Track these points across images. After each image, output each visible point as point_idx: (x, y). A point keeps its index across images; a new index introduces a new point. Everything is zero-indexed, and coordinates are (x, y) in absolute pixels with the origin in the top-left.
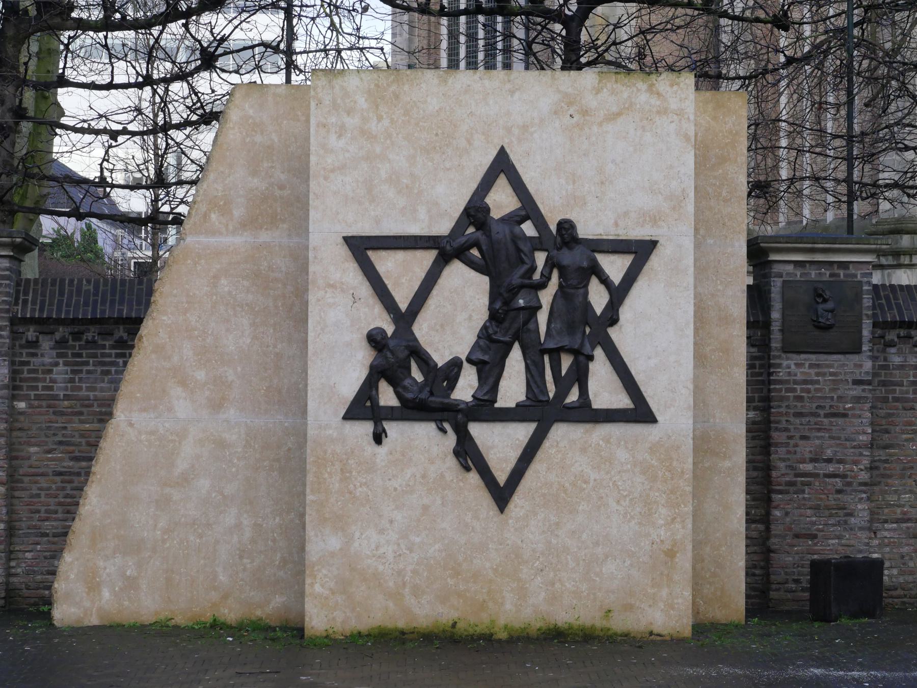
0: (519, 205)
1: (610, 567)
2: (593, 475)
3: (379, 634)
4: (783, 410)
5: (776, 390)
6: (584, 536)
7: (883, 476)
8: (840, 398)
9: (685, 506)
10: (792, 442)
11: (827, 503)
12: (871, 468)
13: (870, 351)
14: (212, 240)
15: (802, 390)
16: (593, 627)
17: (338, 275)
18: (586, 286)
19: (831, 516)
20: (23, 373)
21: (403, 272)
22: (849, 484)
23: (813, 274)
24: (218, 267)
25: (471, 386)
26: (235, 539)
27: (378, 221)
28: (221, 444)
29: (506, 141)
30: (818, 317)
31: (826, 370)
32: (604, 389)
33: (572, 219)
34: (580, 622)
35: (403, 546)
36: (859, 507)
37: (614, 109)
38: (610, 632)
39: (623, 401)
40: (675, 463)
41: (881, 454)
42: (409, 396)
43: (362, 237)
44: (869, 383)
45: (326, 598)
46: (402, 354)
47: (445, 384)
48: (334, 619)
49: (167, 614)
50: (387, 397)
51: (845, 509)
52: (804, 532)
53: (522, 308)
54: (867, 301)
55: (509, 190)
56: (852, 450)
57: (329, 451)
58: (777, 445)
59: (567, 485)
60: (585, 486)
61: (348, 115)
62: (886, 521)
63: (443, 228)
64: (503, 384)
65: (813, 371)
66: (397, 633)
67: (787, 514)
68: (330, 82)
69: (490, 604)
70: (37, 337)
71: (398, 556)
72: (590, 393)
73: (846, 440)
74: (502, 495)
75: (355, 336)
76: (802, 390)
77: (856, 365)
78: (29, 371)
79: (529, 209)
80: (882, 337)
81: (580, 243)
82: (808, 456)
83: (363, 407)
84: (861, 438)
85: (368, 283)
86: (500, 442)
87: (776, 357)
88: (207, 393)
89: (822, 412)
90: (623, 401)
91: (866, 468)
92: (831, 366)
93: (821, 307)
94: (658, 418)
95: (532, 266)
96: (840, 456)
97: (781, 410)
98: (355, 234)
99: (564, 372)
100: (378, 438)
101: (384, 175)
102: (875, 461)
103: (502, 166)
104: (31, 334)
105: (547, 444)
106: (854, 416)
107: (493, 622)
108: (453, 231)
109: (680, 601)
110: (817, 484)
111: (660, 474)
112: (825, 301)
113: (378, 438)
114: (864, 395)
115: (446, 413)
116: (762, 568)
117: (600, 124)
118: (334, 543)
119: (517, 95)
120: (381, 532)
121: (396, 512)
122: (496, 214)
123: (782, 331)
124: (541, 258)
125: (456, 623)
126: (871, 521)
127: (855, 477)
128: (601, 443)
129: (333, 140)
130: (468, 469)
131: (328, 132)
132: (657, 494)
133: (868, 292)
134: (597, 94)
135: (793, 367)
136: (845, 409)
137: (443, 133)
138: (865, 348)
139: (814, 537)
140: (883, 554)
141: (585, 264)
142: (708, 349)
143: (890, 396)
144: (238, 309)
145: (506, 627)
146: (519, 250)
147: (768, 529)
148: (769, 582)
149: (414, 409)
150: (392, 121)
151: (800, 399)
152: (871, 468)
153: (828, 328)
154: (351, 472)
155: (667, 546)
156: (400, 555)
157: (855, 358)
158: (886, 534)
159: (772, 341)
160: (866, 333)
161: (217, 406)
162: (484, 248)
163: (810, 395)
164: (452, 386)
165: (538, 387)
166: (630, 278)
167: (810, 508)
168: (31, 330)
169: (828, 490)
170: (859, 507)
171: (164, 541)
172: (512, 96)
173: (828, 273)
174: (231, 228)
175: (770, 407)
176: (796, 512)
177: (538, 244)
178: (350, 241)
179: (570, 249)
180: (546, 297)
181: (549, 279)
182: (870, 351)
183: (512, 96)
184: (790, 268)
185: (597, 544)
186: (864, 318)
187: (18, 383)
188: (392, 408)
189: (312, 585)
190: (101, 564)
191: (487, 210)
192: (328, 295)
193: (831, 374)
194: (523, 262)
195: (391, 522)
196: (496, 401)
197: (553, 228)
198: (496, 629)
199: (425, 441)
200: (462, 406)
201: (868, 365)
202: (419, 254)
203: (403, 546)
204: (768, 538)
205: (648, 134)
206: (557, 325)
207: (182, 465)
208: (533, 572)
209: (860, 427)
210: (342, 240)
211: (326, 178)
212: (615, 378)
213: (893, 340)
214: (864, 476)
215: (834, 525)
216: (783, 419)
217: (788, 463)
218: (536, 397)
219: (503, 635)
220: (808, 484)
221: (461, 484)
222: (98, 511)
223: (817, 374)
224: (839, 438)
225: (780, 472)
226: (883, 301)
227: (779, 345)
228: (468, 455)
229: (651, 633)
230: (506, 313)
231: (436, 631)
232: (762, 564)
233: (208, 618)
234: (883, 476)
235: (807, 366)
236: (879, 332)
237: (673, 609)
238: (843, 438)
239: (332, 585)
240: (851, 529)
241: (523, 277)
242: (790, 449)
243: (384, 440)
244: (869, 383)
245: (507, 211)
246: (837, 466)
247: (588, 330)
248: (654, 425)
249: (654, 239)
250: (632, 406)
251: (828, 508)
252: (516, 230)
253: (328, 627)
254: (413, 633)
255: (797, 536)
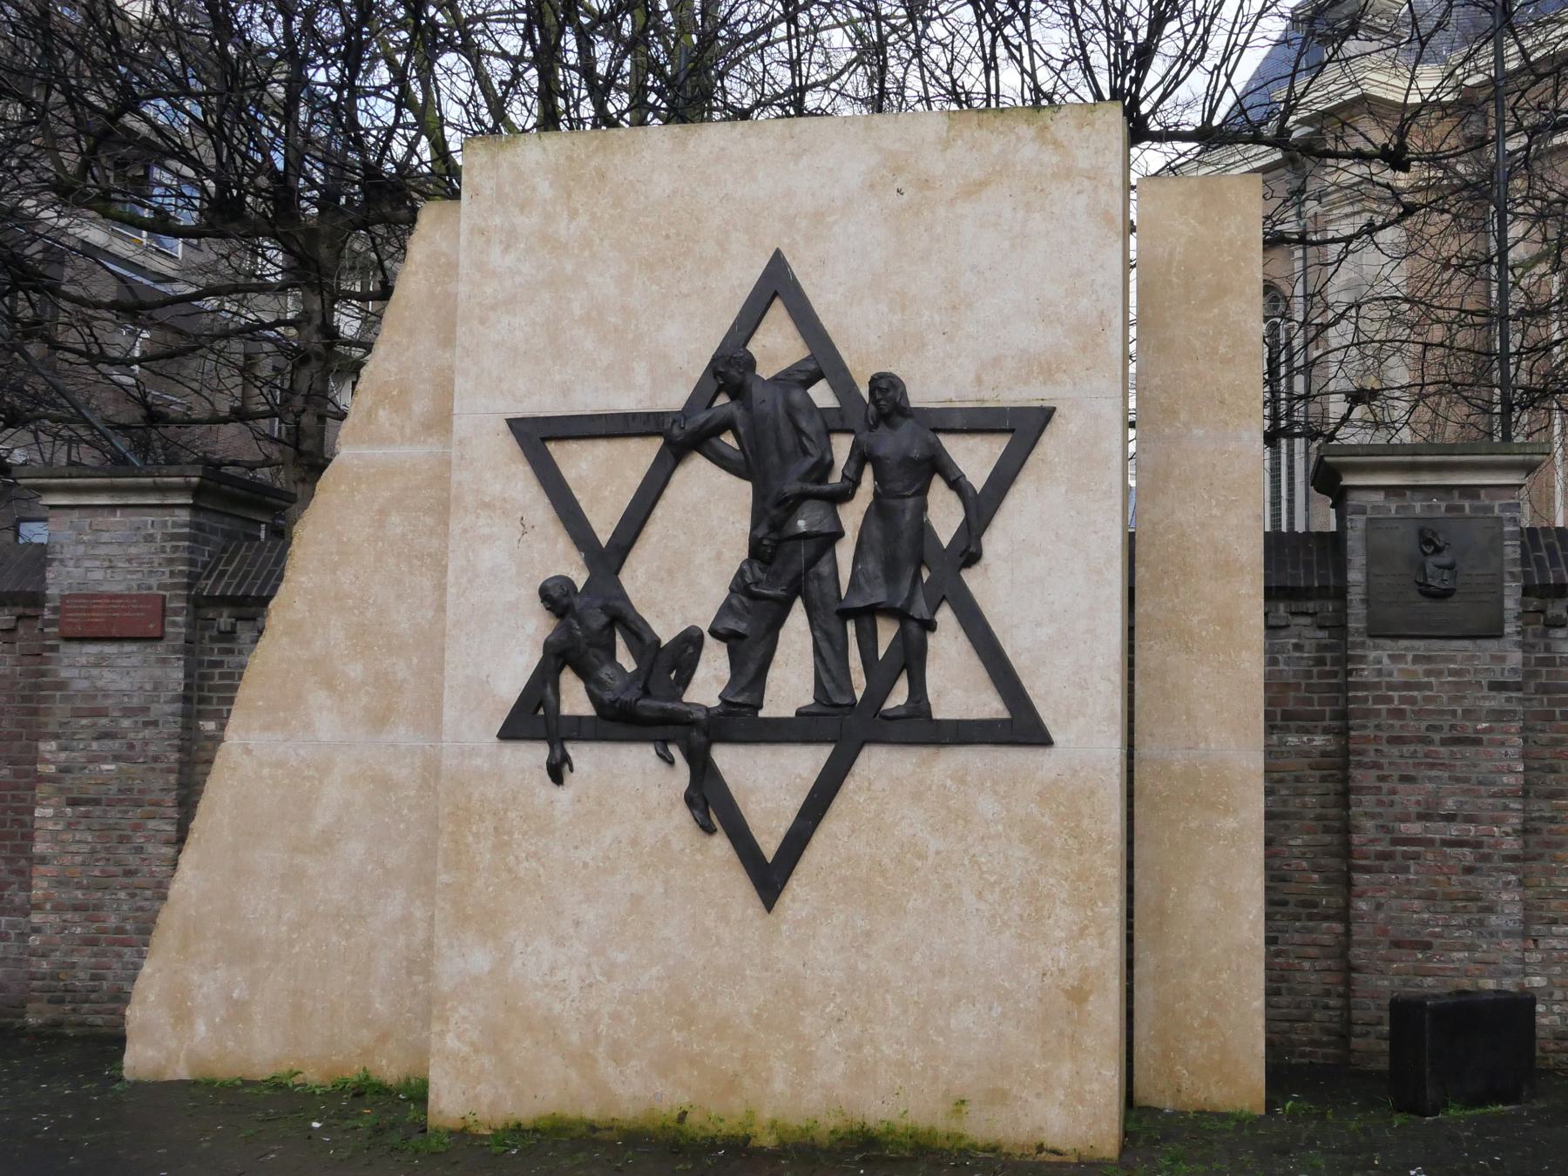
0: (807, 353)
1: (964, 1018)
2: (934, 844)
3: (553, 1128)
4: (1370, 732)
5: (1356, 699)
6: (917, 958)
7: (1548, 845)
8: (1467, 713)
9: (1105, 904)
10: (1385, 786)
11: (1449, 889)
12: (1525, 831)
13: (1518, 633)
14: (379, 452)
15: (1403, 700)
16: (931, 1130)
17: (498, 487)
18: (923, 491)
19: (1455, 911)
20: (212, 678)
21: (604, 476)
22: (1486, 858)
23: (1418, 508)
24: (387, 494)
25: (716, 678)
26: (401, 941)
27: (565, 389)
28: (385, 784)
29: (786, 241)
30: (1425, 578)
31: (1442, 666)
32: (954, 683)
33: (898, 373)
34: (907, 1122)
35: (595, 969)
36: (1505, 897)
37: (976, 175)
38: (963, 1144)
39: (991, 706)
40: (1086, 823)
41: (1542, 808)
42: (608, 696)
43: (536, 420)
44: (1518, 687)
45: (465, 1060)
46: (598, 620)
47: (673, 676)
48: (476, 1097)
49: (292, 1064)
50: (575, 699)
51: (1479, 899)
52: (1408, 937)
53: (804, 536)
54: (1512, 551)
55: (789, 327)
56: (1490, 801)
57: (476, 795)
58: (1360, 790)
59: (886, 861)
60: (919, 864)
61: (522, 209)
62: (1554, 922)
63: (674, 398)
64: (774, 674)
65: (1420, 668)
66: (584, 1129)
67: (1379, 907)
68: (493, 157)
69: (747, 1081)
70: (233, 626)
71: (587, 986)
72: (929, 691)
73: (1480, 783)
74: (769, 877)
75: (523, 592)
76: (1403, 700)
77: (1493, 657)
78: (222, 676)
79: (822, 360)
80: (1542, 611)
81: (911, 416)
82: (1413, 809)
83: (532, 718)
84: (1505, 780)
85: (547, 500)
86: (768, 781)
87: (1355, 645)
88: (365, 700)
89: (1437, 737)
90: (991, 706)
91: (1515, 831)
92: (1452, 660)
93: (1431, 562)
94: (1054, 737)
95: (822, 458)
96: (1468, 810)
97: (1367, 732)
98: (527, 415)
99: (881, 653)
100: (557, 771)
101: (577, 310)
102: (1532, 819)
103: (778, 285)
104: (224, 621)
105: (850, 784)
106: (1492, 742)
107: (750, 1114)
108: (690, 402)
109: (1096, 1087)
110: (1430, 856)
111: (1058, 843)
112: (1438, 550)
113: (557, 771)
114: (1508, 707)
115: (670, 728)
116: (1340, 996)
117: (952, 202)
118: (480, 960)
119: (805, 161)
120: (560, 942)
121: (584, 906)
122: (766, 370)
123: (1366, 602)
124: (842, 447)
125: (685, 1113)
126: (1526, 922)
127: (1497, 845)
128: (949, 782)
129: (496, 258)
130: (709, 830)
131: (488, 241)
132: (1052, 881)
133: (1512, 535)
134: (944, 150)
135: (1386, 660)
136: (1477, 731)
137: (678, 234)
138: (1509, 629)
139: (1427, 946)
140: (1549, 977)
141: (916, 453)
142: (1195, 620)
143: (1557, 710)
144: (415, 561)
145: (773, 1124)
146: (799, 431)
147: (1348, 933)
148: (1349, 1023)
149: (619, 721)
150: (593, 217)
151: (1399, 714)
152: (1525, 831)
153: (1444, 595)
154: (510, 833)
155: (1070, 981)
156: (590, 985)
157: (1491, 645)
158: (1555, 943)
159: (1351, 618)
160: (1511, 603)
161: (379, 720)
162: (741, 430)
163: (1416, 708)
164: (685, 680)
165: (833, 679)
166: (1004, 477)
167: (1418, 898)
168: (225, 614)
169: (1450, 867)
170: (1505, 897)
171: (291, 944)
172: (796, 163)
173: (1443, 505)
174: (408, 431)
175: (1349, 729)
176: (1395, 903)
177: (832, 423)
178: (518, 426)
179: (892, 426)
180: (852, 516)
181: (856, 483)
182: (1518, 633)
183: (796, 163)
184: (1378, 498)
185: (939, 973)
186: (1507, 577)
187: (206, 694)
188: (580, 718)
189: (442, 1034)
190: (195, 977)
191: (751, 363)
192: (482, 522)
193: (1452, 673)
194: (806, 452)
195: (577, 924)
196: (761, 707)
197: (864, 391)
198: (756, 1129)
199: (633, 780)
200: (701, 715)
201: (1515, 658)
202: (634, 445)
203: (595, 969)
204: (1348, 947)
205: (1037, 215)
206: (872, 565)
207: (322, 818)
208: (823, 1022)
209: (1505, 762)
210: (505, 426)
211: (482, 322)
212: (974, 661)
213: (1559, 616)
214: (1512, 845)
215: (1460, 927)
216: (1371, 748)
217: (1380, 822)
218: (828, 698)
219: (768, 1141)
220: (1415, 857)
221: (699, 857)
222: (193, 892)
223: (1428, 673)
224: (1466, 780)
225: (1367, 834)
226: (1544, 553)
227: (1361, 625)
228: (710, 802)
229: (1040, 1148)
230: (778, 544)
231: (651, 1127)
232: (1341, 989)
233: (353, 1073)
234: (1548, 845)
235: (1410, 658)
236: (1535, 603)
237: (1082, 1101)
238: (1474, 780)
239: (475, 1035)
240: (1491, 935)
241: (805, 478)
242: (1384, 798)
243: (568, 778)
244: (1518, 687)
245: (785, 364)
246: (1465, 826)
247: (925, 575)
248: (1048, 750)
249: (1046, 404)
250: (1006, 715)
251: (1449, 897)
252: (796, 396)
253: (466, 1113)
254: (611, 1128)
255: (1397, 944)
